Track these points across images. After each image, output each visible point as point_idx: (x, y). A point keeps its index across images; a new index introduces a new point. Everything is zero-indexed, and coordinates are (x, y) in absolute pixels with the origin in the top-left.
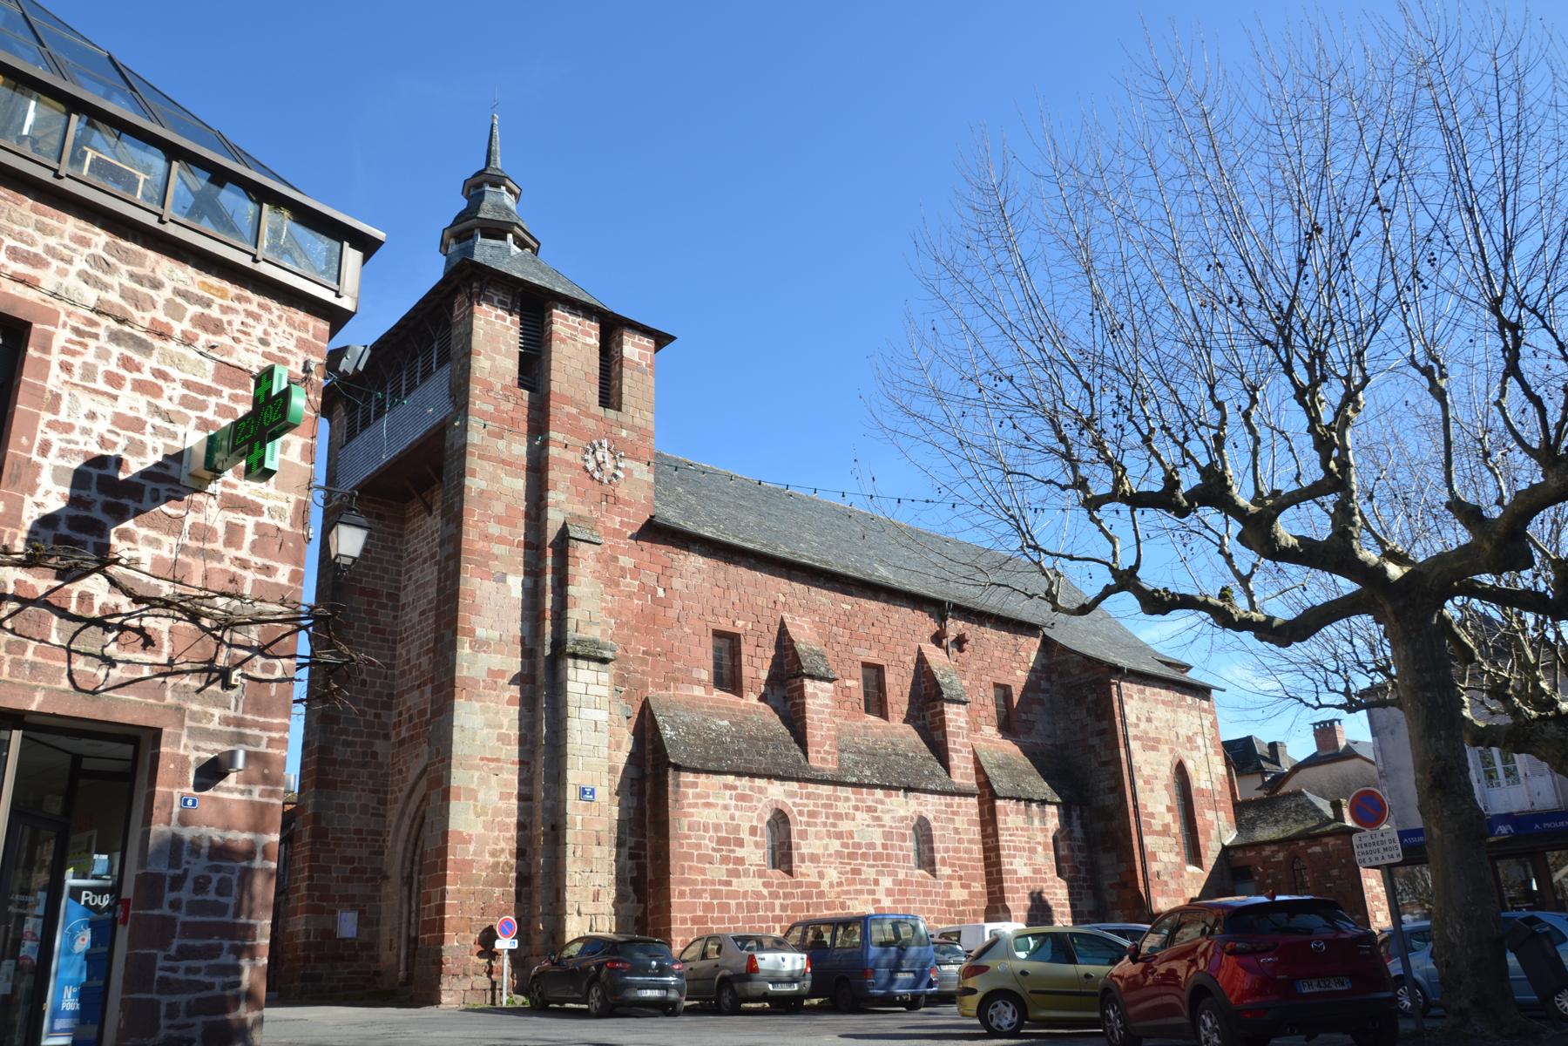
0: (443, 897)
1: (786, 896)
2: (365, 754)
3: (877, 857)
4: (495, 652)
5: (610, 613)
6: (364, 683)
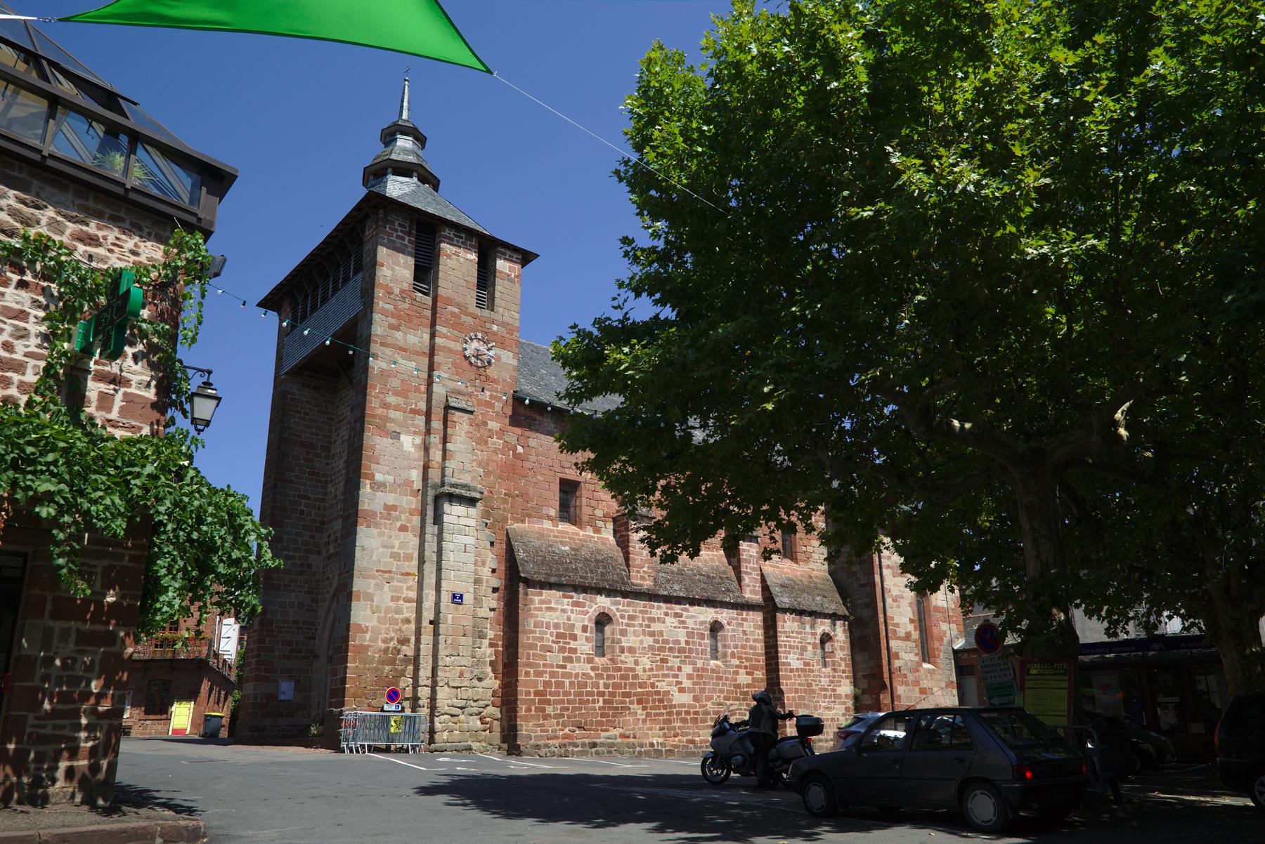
2: (302, 565)
3: (681, 650)
4: (391, 492)
6: (302, 512)
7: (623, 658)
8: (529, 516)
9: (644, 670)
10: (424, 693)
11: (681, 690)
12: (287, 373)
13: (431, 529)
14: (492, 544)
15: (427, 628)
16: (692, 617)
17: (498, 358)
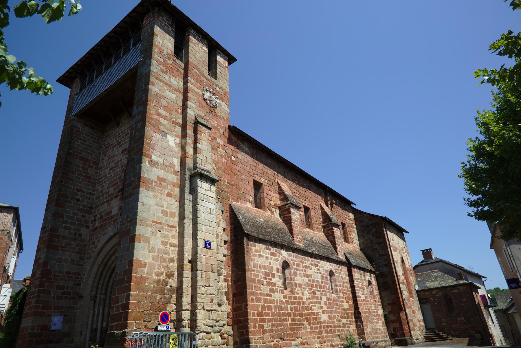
0: (128, 298)
1: (292, 303)
2: (75, 234)
3: (320, 287)
4: (162, 169)
5: (214, 162)
6: (78, 200)
7: (296, 291)
8: (240, 198)
9: (307, 299)
10: (186, 315)
11: (323, 312)
12: (75, 115)
13: (188, 197)
14: (222, 211)
15: (187, 267)
16: (322, 267)
17: (220, 105)
